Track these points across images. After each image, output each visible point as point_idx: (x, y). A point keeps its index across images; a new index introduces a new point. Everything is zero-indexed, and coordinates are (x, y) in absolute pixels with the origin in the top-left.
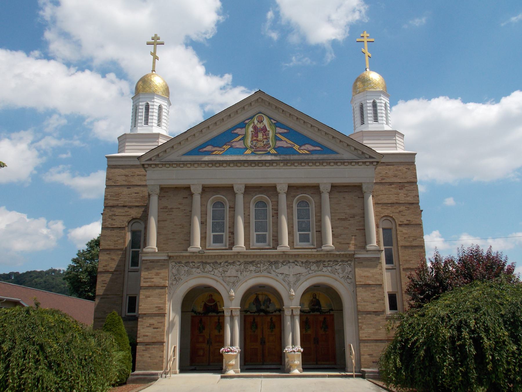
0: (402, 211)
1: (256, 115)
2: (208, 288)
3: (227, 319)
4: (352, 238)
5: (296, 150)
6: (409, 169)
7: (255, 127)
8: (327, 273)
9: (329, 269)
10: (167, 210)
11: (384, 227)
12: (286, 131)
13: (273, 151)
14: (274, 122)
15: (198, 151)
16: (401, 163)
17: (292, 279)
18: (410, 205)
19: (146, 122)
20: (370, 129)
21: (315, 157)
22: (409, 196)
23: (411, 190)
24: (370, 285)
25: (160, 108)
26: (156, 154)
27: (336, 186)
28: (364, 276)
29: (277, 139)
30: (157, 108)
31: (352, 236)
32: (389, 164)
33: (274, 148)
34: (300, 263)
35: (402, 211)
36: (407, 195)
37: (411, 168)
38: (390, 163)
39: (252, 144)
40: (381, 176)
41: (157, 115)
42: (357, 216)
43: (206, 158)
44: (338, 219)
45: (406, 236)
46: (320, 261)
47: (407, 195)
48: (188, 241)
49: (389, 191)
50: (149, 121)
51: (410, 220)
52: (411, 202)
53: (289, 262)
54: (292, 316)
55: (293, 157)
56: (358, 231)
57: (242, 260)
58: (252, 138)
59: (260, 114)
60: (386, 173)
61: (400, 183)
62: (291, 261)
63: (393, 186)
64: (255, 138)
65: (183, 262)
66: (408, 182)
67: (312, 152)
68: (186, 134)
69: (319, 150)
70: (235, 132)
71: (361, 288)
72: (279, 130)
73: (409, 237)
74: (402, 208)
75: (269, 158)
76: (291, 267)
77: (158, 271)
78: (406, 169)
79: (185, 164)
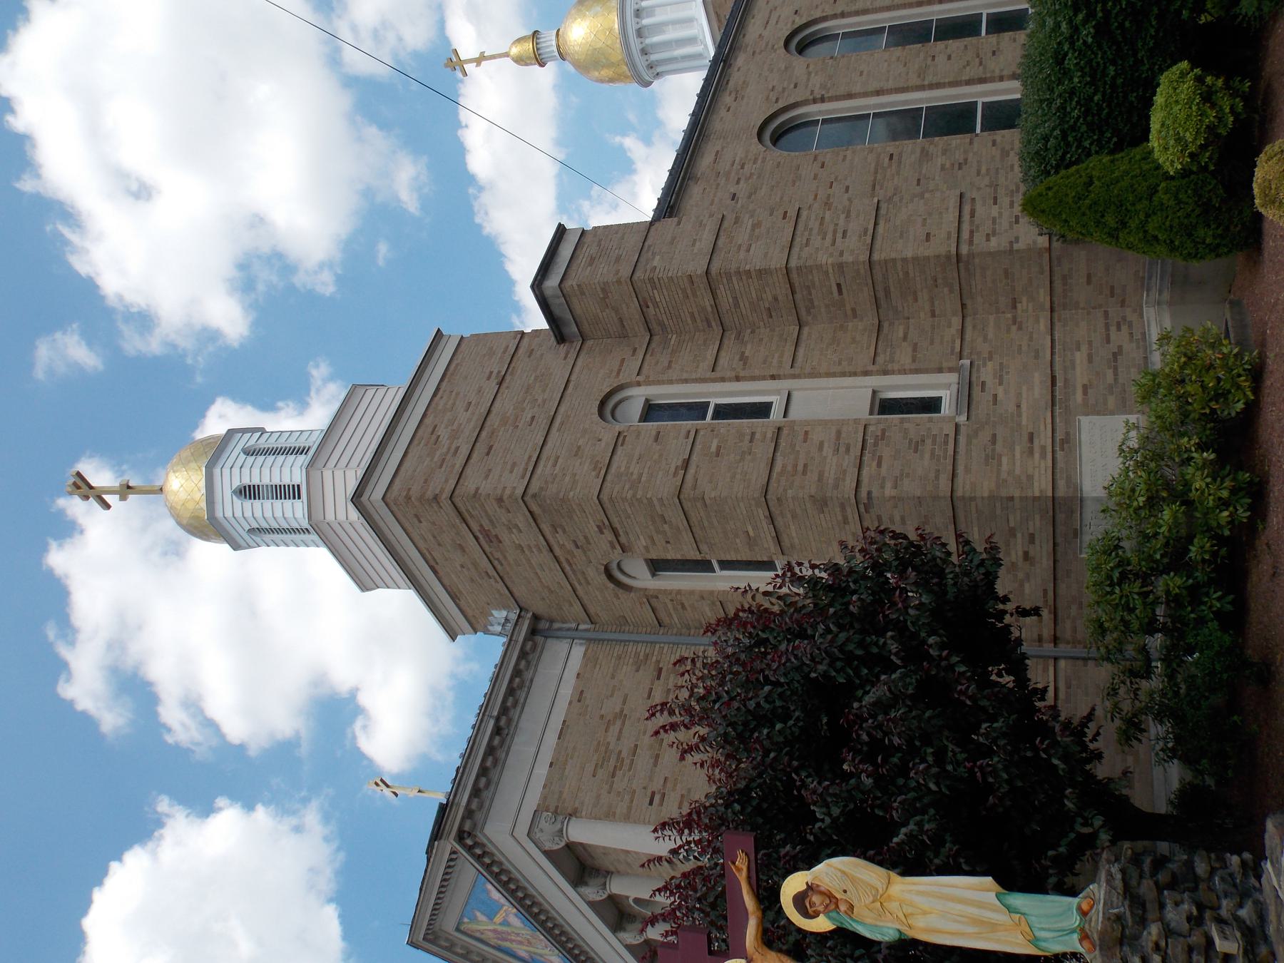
0: (575, 542)
22: (509, 521)
27: (578, 859)
52: (531, 520)
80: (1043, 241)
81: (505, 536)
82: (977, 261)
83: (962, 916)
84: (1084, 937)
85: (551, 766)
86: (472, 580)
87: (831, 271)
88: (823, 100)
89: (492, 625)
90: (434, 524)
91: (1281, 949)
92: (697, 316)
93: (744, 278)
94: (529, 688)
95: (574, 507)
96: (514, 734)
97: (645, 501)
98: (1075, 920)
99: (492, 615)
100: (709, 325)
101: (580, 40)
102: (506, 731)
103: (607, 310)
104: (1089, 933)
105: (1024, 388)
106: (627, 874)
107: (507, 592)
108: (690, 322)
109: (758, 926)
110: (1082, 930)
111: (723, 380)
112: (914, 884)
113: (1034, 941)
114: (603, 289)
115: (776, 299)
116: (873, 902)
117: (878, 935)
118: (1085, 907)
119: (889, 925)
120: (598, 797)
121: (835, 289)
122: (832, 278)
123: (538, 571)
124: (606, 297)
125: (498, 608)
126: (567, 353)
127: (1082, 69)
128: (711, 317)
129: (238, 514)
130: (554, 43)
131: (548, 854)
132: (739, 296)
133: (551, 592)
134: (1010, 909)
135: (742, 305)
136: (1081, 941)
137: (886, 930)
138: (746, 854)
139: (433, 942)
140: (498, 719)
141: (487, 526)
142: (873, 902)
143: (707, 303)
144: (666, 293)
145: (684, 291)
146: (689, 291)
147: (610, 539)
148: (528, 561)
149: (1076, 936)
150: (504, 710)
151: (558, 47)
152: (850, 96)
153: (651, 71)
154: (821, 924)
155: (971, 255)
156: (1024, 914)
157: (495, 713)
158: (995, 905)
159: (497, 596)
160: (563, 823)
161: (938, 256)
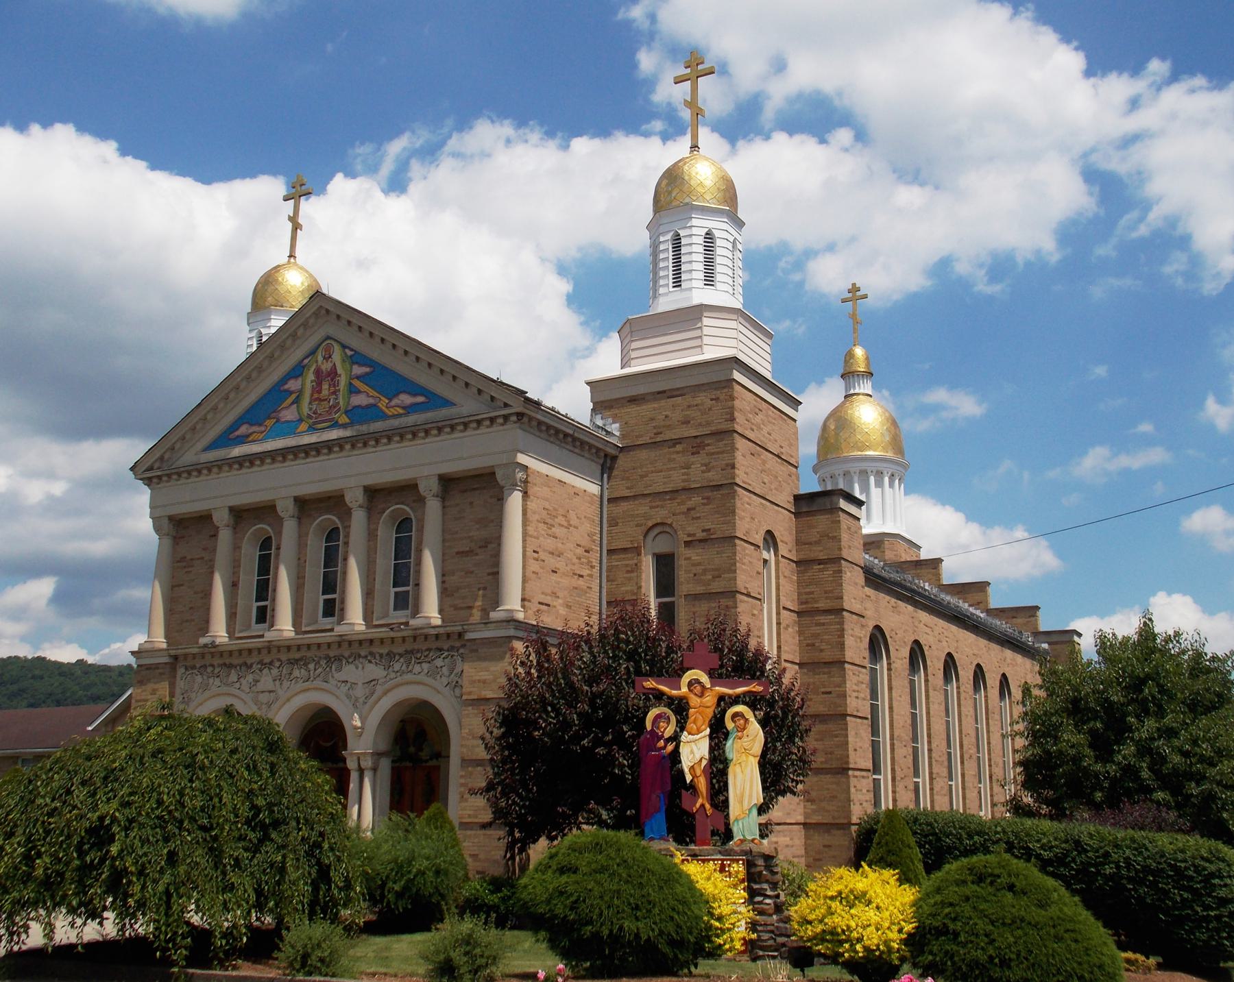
0: (694, 509)
1: (320, 345)
2: (425, 705)
3: (354, 776)
4: (477, 595)
5: (382, 411)
6: (717, 399)
7: (318, 372)
8: (422, 678)
9: (425, 666)
10: (184, 564)
11: (657, 551)
12: (368, 370)
13: (344, 419)
14: (349, 353)
15: (227, 438)
16: (699, 387)
17: (360, 692)
18: (712, 491)
19: (678, 283)
20: (660, 309)
21: (411, 419)
22: (713, 467)
23: (718, 453)
24: (488, 699)
25: (709, 237)
26: (158, 455)
27: (458, 479)
28: (479, 681)
29: (353, 390)
30: (701, 240)
31: (479, 589)
32: (675, 393)
33: (346, 412)
34: (377, 656)
35: (694, 509)
36: (708, 467)
37: (722, 397)
38: (678, 389)
39: (310, 409)
40: (655, 427)
41: (703, 260)
42: (491, 543)
43: (237, 451)
44: (458, 553)
45: (699, 569)
46: (412, 652)
47: (708, 467)
48: (204, 625)
49: (670, 460)
50: (684, 277)
51: (709, 530)
52: (714, 483)
53: (360, 656)
54: (361, 771)
55: (378, 426)
56: (490, 577)
57: (284, 657)
58: (312, 395)
59: (328, 342)
60: (666, 416)
61: (696, 437)
62: (363, 653)
63: (679, 448)
64: (316, 396)
65: (198, 666)
66: (713, 434)
67: (409, 409)
68: (202, 407)
69: (423, 403)
70: (286, 387)
71: (470, 708)
72: (358, 370)
73: (705, 571)
74: (696, 500)
75: (334, 434)
76: (360, 666)
77: (156, 686)
78: (712, 400)
79: (210, 467)
80: (855, 820)
84: (742, 841)
86: (652, 419)
88: (889, 669)
90: (710, 409)
91: (272, 973)
98: (749, 838)
99: (614, 422)
100: (802, 603)
101: (857, 414)
106: (444, 514)
111: (778, 613)
113: (737, 820)
115: (822, 651)
121: (829, 690)
125: (621, 429)
127: (974, 845)
128: (810, 606)
129: (694, 231)
130: (862, 391)
133: (642, 477)
134: (750, 810)
139: (316, 314)
140: (572, 436)
145: (831, 591)
148: (674, 469)
150: (575, 439)
151: (858, 394)
152: (890, 689)
153: (829, 477)
154: (730, 725)
155: (848, 777)
157: (576, 435)
161: (848, 757)
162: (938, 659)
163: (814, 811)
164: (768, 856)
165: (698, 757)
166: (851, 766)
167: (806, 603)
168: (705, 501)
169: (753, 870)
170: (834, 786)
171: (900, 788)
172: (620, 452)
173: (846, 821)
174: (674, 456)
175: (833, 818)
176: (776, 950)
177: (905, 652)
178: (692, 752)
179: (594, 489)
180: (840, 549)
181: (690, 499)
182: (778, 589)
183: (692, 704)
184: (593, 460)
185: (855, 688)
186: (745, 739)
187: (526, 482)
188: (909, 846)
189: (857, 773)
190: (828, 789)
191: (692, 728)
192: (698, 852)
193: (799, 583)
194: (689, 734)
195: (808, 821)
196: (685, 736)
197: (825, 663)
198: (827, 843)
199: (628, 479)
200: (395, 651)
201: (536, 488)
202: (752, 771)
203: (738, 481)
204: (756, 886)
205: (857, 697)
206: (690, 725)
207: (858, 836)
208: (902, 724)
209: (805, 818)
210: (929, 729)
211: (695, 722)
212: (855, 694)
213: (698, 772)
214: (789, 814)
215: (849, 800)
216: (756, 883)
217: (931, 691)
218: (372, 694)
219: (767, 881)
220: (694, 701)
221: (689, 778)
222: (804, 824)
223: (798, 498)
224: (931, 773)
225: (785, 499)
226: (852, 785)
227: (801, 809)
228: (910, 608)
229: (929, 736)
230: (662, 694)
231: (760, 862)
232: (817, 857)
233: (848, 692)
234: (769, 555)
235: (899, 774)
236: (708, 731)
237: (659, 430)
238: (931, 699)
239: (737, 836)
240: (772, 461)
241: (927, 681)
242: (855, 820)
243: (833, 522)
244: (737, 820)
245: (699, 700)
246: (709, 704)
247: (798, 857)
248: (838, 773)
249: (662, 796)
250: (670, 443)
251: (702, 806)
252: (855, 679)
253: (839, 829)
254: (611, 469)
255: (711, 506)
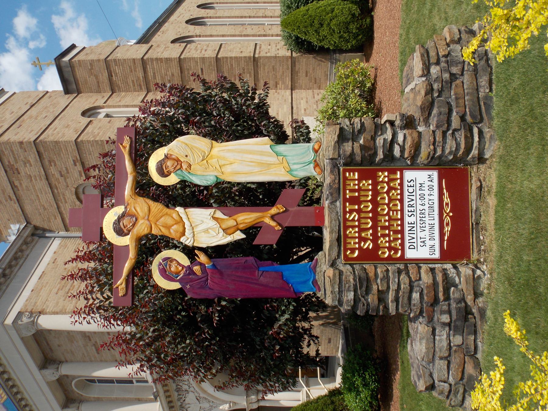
0: (60, 172)
18: (44, 159)
22: (25, 158)
23: (13, 154)
27: (43, 353)
36: (26, 162)
40: (7, 201)
47: (26, 162)
51: (74, 161)
52: (38, 157)
61: (6, 171)
63: (17, 183)
74: (53, 170)
76: (188, 406)
80: (289, 54)
81: (22, 170)
82: (261, 60)
83: (251, 162)
84: (317, 165)
85: (32, 291)
87: (199, 61)
88: (200, 36)
89: (10, 236)
92: (135, 83)
93: (159, 62)
94: (26, 259)
95: (62, 147)
96: (14, 278)
97: (100, 143)
98: (312, 155)
99: (10, 228)
100: (141, 89)
102: (8, 277)
103: (92, 77)
104: (319, 163)
105: (280, 109)
106: (72, 362)
107: (20, 210)
108: (132, 86)
109: (133, 181)
110: (315, 161)
112: (226, 146)
113: (290, 171)
114: (91, 64)
115: (173, 75)
116: (203, 160)
117: (205, 181)
118: (316, 147)
119: (211, 173)
120: (57, 303)
122: (199, 65)
123: (39, 194)
124: (92, 69)
125: (14, 223)
126: (68, 98)
131: (22, 339)
132: (156, 72)
133: (45, 209)
134: (277, 154)
135: (157, 78)
136: (314, 168)
137: (208, 177)
138: (130, 138)
141: (12, 161)
142: (203, 160)
143: (141, 76)
144: (121, 68)
145: (130, 67)
146: (133, 68)
147: (79, 169)
148: (34, 186)
149: (312, 165)
154: (172, 180)
155: (260, 57)
156: (285, 156)
158: (269, 152)
159: (15, 214)
160: (35, 318)
161: (245, 57)
162: (199, 11)
163: (284, 83)
164: (339, 136)
165: (213, 223)
166: (252, 55)
167: (140, 85)
168: (53, 164)
169: (358, 158)
170: (266, 68)
171: (270, 32)
172: (31, 224)
173: (290, 60)
174: (24, 186)
175: (288, 69)
176: (471, 131)
177: (191, 27)
178: (206, 231)
179: (57, 243)
180: (99, 60)
181: (53, 175)
182: (127, 106)
183: (146, 231)
184: (34, 246)
185: (199, 51)
186: (191, 159)
187: (31, 313)
188: (308, 10)
189: (257, 51)
190: (268, 72)
191: (176, 231)
192: (335, 235)
193: (127, 90)
194: (183, 234)
195: (290, 87)
196: (187, 241)
197: (181, 72)
198: (304, 74)
199: (48, 218)
200: (175, 387)
201: (38, 303)
202: (229, 151)
203: (33, 139)
204: (380, 155)
205: (206, 50)
206: (173, 232)
207: (300, 52)
208: (233, 30)
209: (288, 89)
210: (238, 17)
211: (168, 227)
212: (203, 52)
213: (231, 222)
214: (285, 101)
215: (276, 57)
216: (375, 154)
217: (217, 15)
218: (206, 399)
219: (373, 139)
220: (142, 228)
221: (239, 236)
222: (292, 90)
223: (67, 91)
224: (263, 17)
225: (65, 100)
226: (265, 55)
227: (282, 92)
228: (166, 24)
229: (242, 17)
230: (132, 272)
231: (348, 147)
232: (313, 81)
233: (201, 56)
234: (103, 112)
235: (262, 33)
236: (179, 209)
237: (8, 197)
238: (221, 15)
239: (310, 171)
240: (33, 111)
241: (210, 18)
242: (289, 54)
243: (80, 66)
244: (290, 171)
245: (141, 222)
246: (146, 209)
247: (313, 94)
248: (257, 66)
249: (261, 269)
250: (15, 189)
251: (273, 217)
252: (193, 51)
253: (295, 66)
254: (45, 230)
255: (56, 159)
